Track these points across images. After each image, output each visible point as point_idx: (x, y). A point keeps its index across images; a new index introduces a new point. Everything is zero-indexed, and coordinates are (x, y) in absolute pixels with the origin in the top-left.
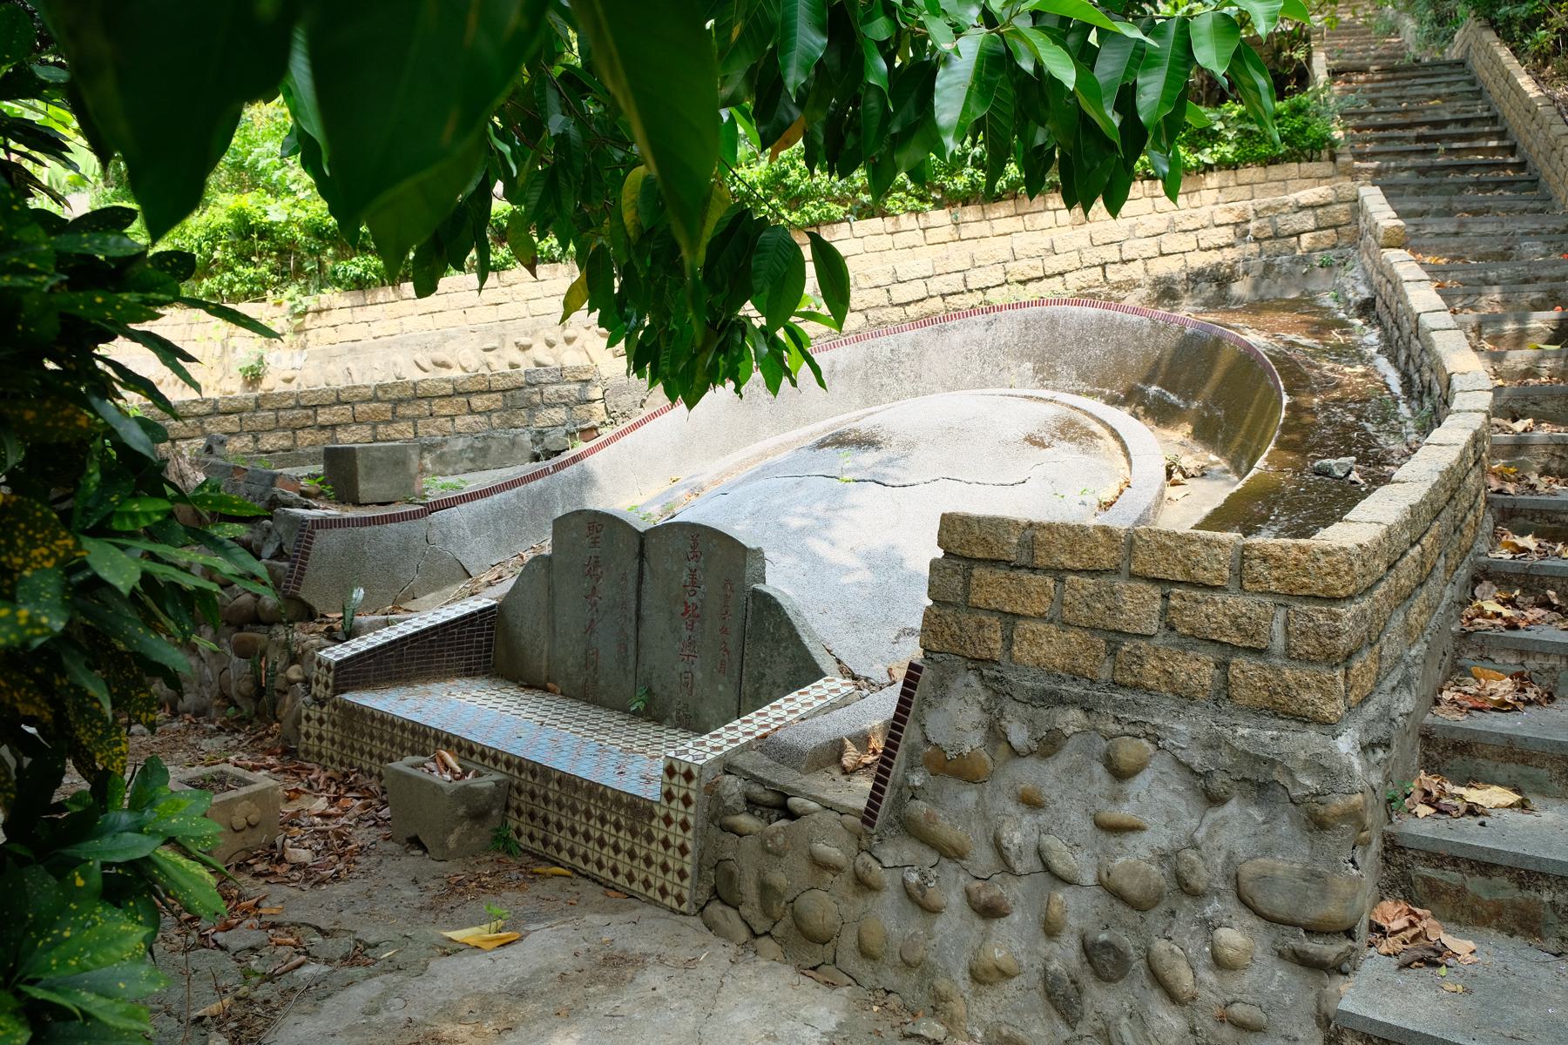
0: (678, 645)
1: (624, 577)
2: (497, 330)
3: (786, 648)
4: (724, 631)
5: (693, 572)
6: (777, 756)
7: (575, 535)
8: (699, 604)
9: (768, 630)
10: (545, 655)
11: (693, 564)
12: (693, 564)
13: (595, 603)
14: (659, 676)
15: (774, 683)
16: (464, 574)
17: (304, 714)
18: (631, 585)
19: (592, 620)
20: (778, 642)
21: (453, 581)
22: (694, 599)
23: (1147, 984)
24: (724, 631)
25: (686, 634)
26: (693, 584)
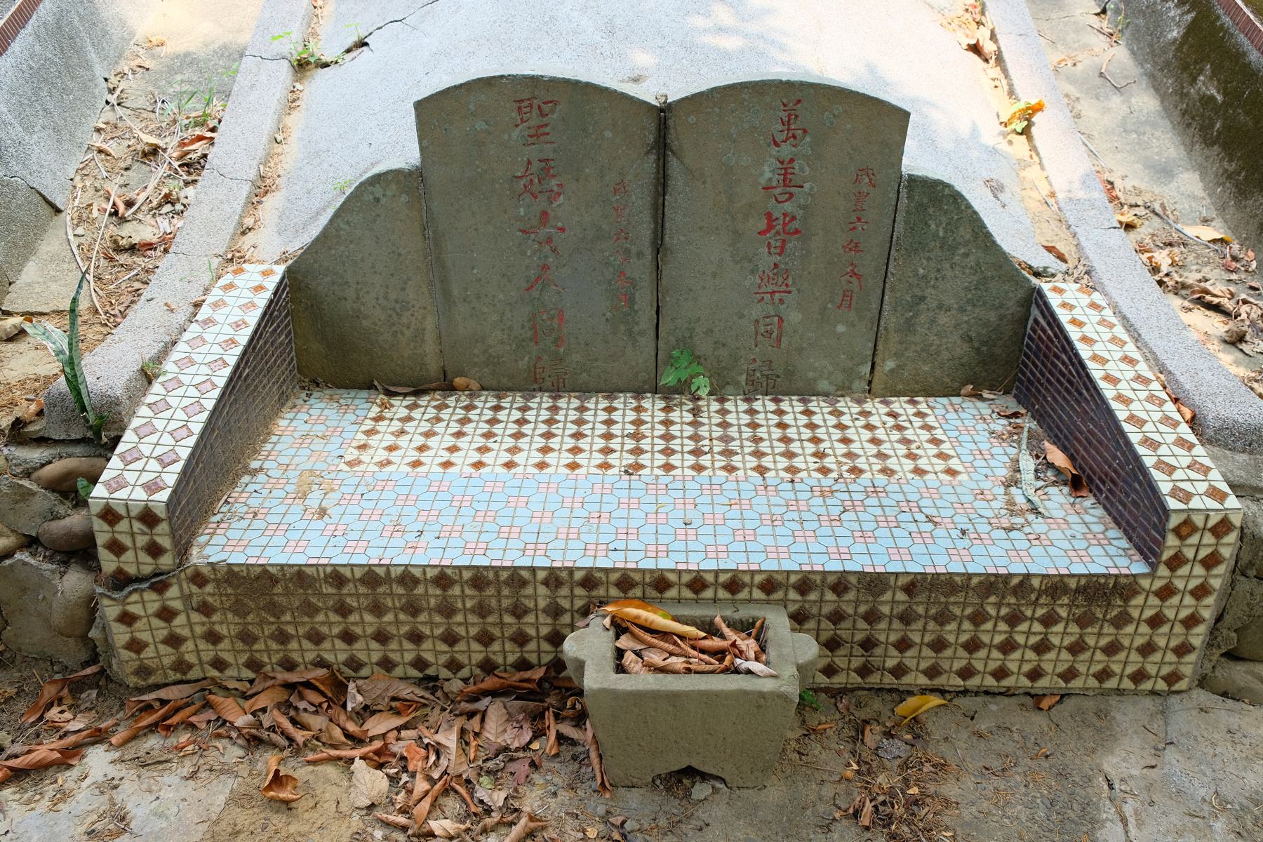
0: (751, 281)
1: (620, 187)
2: (1047, 213)
3: (966, 255)
4: (854, 247)
5: (786, 168)
6: (1239, 445)
7: (480, 125)
8: (799, 214)
9: (935, 235)
10: (430, 337)
11: (786, 150)
12: (786, 150)
13: (549, 240)
14: (710, 332)
15: (940, 307)
16: (48, 210)
17: (101, 539)
18: (640, 199)
19: (545, 267)
20: (953, 249)
21: (39, 231)
22: (788, 207)
23: (74, 773)
24: (854, 247)
25: (766, 260)
26: (786, 182)
